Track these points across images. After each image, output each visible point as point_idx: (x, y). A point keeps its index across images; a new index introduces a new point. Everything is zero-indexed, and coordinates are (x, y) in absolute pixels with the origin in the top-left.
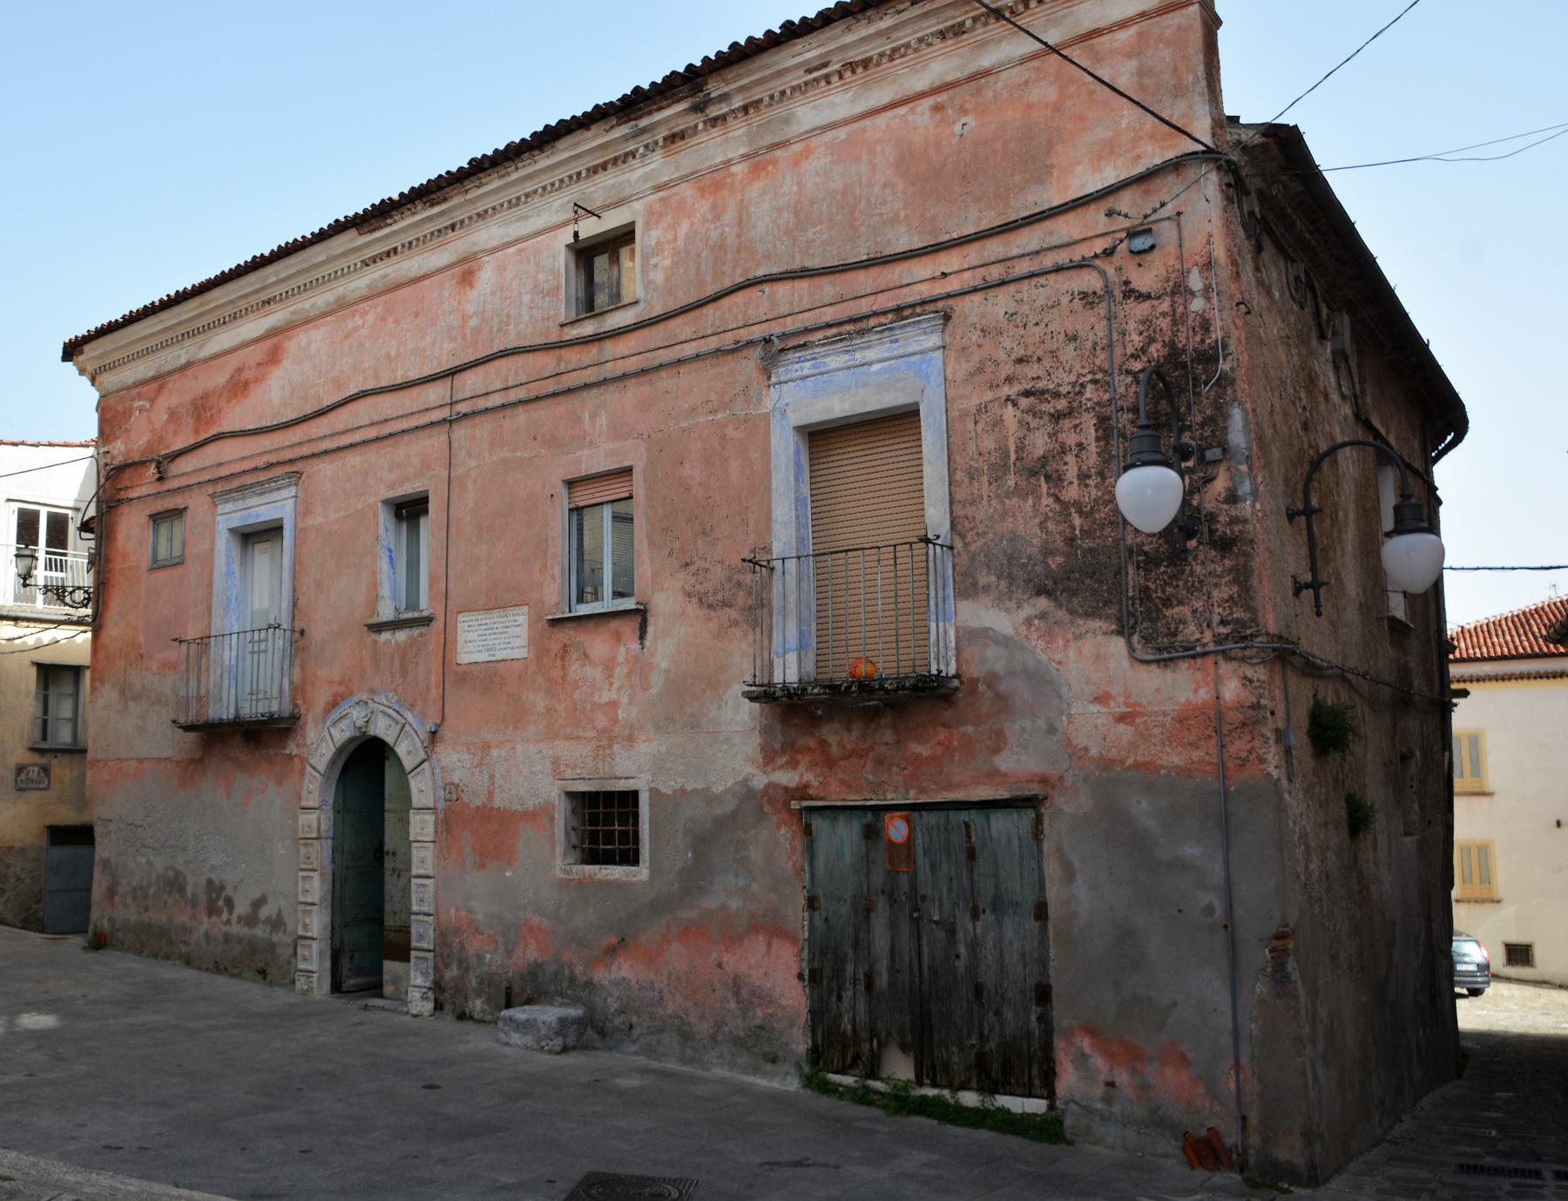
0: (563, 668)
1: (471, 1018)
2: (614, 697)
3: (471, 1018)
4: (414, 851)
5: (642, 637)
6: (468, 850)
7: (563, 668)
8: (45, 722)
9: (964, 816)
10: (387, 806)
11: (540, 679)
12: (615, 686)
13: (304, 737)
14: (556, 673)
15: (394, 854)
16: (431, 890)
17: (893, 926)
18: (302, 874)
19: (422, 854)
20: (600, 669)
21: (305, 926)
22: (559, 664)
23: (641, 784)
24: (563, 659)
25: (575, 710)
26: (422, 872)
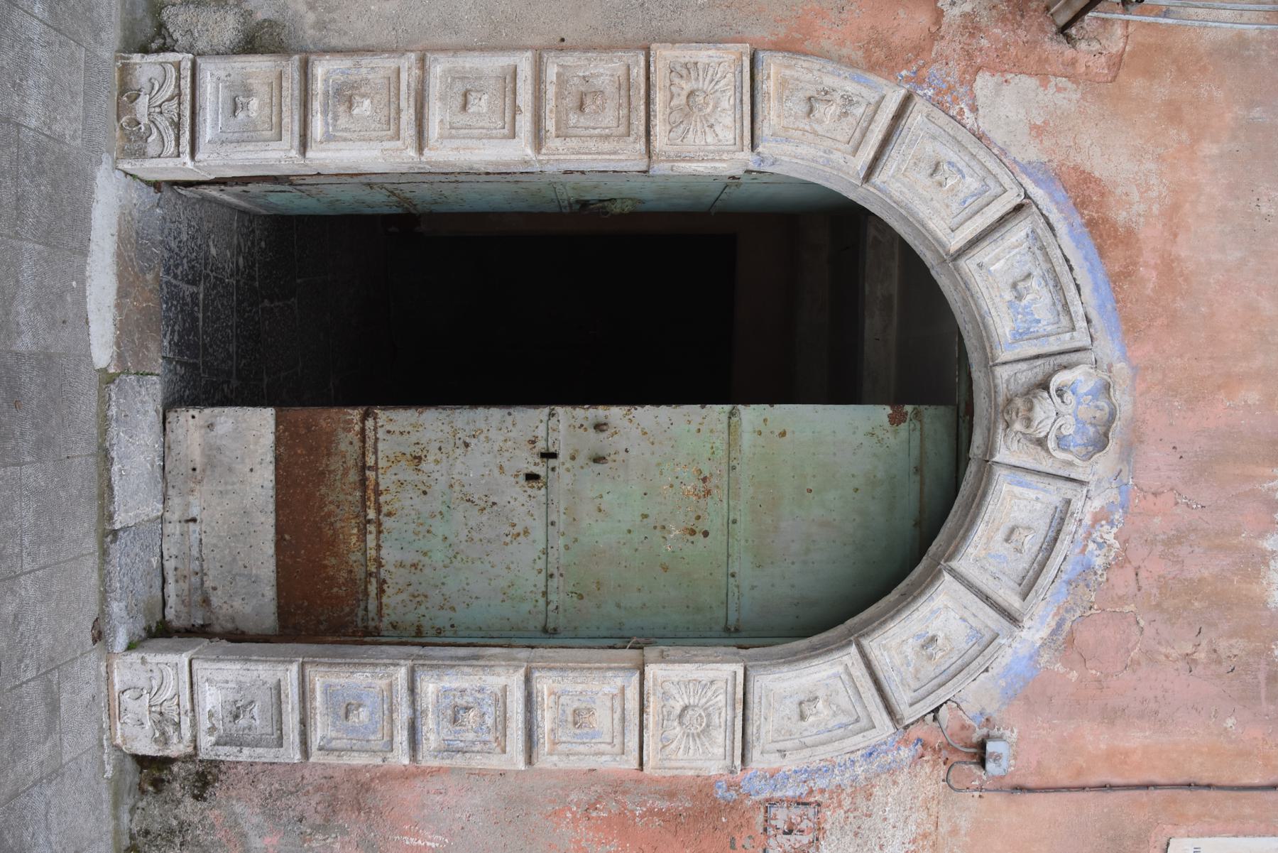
8: (1198, 786)
10: (751, 414)
13: (1003, 64)
16: (495, 762)
18: (524, 64)
19: (603, 719)
21: (345, 95)
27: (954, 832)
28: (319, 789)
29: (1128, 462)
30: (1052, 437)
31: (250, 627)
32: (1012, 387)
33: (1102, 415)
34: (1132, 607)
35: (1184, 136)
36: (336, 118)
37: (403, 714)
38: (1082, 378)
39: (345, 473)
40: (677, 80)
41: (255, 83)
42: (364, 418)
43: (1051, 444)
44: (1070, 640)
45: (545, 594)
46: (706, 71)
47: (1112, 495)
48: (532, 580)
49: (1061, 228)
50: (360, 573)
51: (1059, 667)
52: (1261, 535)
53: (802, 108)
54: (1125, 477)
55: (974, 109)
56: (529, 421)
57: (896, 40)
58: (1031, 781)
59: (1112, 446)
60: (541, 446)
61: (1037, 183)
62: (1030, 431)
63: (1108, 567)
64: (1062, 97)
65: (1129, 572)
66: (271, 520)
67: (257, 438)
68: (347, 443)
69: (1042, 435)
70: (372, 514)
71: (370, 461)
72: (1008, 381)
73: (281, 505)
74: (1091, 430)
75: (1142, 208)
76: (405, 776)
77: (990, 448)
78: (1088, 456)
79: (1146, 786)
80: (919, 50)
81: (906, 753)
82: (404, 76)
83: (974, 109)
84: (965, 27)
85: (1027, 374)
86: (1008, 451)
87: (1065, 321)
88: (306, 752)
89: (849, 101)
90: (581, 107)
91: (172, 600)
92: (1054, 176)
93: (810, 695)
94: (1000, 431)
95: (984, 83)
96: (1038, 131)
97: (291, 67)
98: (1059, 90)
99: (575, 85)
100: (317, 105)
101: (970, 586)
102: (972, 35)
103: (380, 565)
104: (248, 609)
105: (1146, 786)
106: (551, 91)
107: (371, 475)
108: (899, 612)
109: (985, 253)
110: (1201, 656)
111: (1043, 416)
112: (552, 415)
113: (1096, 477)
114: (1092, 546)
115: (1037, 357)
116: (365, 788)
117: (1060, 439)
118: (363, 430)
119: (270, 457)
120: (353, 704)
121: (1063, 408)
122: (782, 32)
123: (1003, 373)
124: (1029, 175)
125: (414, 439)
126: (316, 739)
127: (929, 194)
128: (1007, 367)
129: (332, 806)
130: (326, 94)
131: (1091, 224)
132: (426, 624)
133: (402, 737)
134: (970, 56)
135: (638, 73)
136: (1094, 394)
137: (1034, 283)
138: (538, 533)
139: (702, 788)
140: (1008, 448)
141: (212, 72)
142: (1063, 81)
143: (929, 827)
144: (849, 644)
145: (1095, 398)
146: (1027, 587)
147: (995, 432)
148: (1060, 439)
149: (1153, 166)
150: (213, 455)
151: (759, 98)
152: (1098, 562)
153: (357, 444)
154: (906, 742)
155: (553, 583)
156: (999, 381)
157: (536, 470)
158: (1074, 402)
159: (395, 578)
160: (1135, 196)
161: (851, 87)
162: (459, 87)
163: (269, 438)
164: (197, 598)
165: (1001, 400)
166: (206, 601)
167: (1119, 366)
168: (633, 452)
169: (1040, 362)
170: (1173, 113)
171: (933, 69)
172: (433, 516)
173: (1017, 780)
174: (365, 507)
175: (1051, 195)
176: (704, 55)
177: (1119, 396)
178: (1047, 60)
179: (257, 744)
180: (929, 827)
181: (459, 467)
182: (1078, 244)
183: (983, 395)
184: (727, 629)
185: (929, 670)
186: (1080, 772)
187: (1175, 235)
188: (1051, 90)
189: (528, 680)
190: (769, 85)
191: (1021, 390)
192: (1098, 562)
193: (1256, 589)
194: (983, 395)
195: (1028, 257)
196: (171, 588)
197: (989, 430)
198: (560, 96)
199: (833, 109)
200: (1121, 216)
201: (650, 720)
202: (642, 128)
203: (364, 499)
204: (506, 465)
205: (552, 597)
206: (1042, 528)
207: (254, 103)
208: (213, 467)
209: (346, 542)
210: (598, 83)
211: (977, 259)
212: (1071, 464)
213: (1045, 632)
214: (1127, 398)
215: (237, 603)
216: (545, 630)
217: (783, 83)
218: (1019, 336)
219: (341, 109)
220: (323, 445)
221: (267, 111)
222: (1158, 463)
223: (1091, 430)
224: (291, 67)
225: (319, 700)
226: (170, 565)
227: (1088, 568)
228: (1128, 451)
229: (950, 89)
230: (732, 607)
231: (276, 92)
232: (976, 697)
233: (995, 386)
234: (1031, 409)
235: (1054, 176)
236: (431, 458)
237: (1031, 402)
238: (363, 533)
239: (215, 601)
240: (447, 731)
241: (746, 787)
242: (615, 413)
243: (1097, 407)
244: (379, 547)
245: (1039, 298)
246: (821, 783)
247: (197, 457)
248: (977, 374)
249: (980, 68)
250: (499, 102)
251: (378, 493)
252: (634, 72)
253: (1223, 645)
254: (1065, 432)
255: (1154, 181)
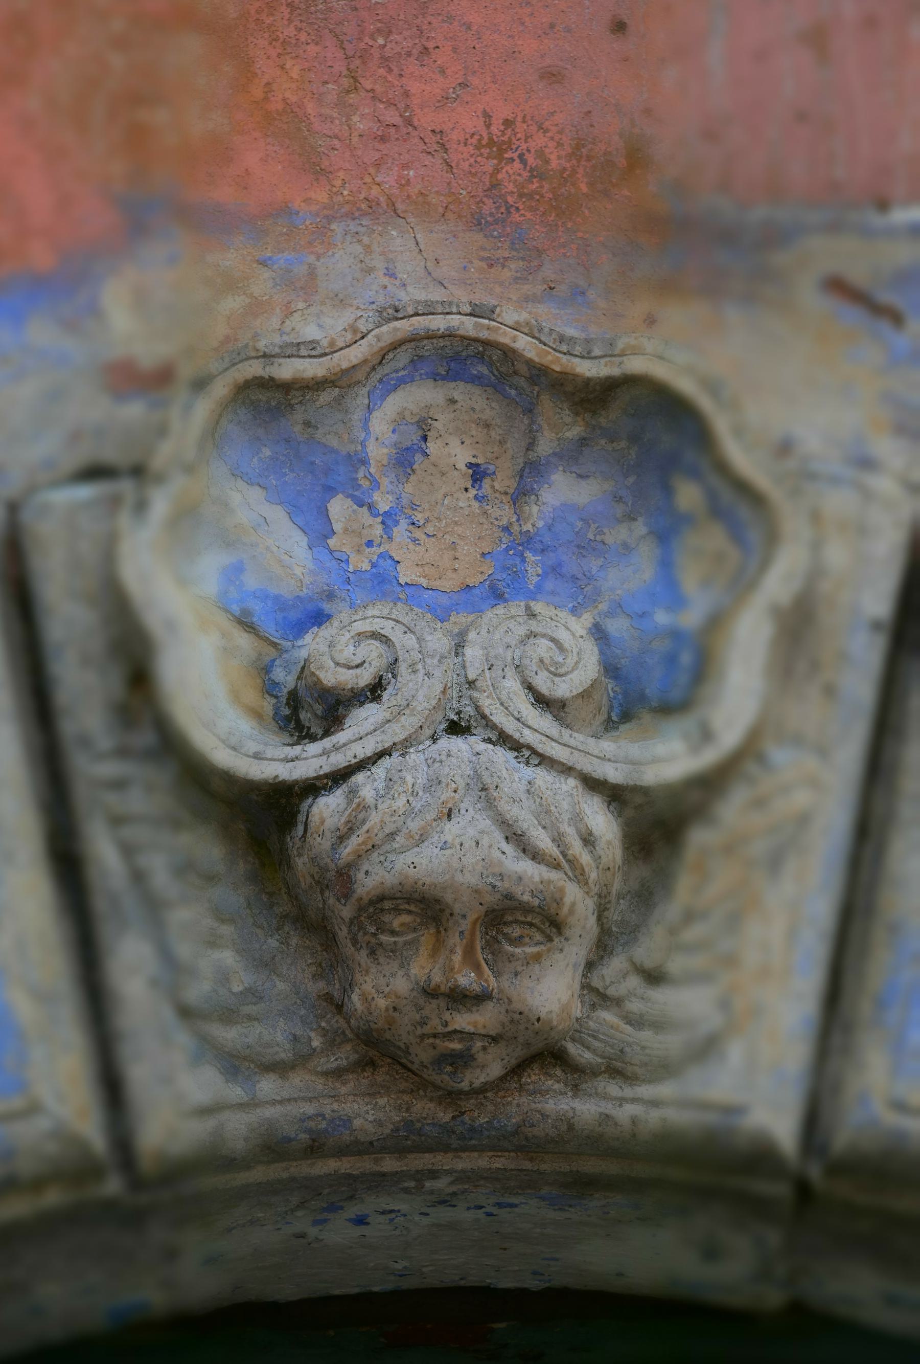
29: (775, 237)
30: (621, 757)
32: (274, 1035)
34: (497, 636)
38: (210, 567)
43: (664, 758)
59: (668, 349)
62: (578, 903)
69: (602, 821)
72: (235, 1064)
74: (562, 492)
77: (710, 1172)
78: (743, 510)
85: (187, 939)
94: (585, 1109)
111: (471, 828)
113: (889, 450)
115: (67, 862)
117: (631, 698)
121: (421, 690)
123: (183, 1100)
128: (140, 1074)
136: (316, 482)
140: (707, 1049)
145: (341, 473)
147: (597, 1142)
148: (631, 698)
156: (238, 1128)
158: (375, 617)
165: (366, 1112)
167: (126, 316)
169: (103, 851)
177: (327, 328)
183: (338, 1232)
191: (296, 977)
194: (338, 1232)
197: (583, 1185)
212: (798, 626)
214: (339, 262)
223: (562, 492)
228: (701, 243)
233: (273, 1148)
234: (426, 907)
237: (382, 903)
243: (404, 460)
248: (194, 1270)
254: (581, 671)
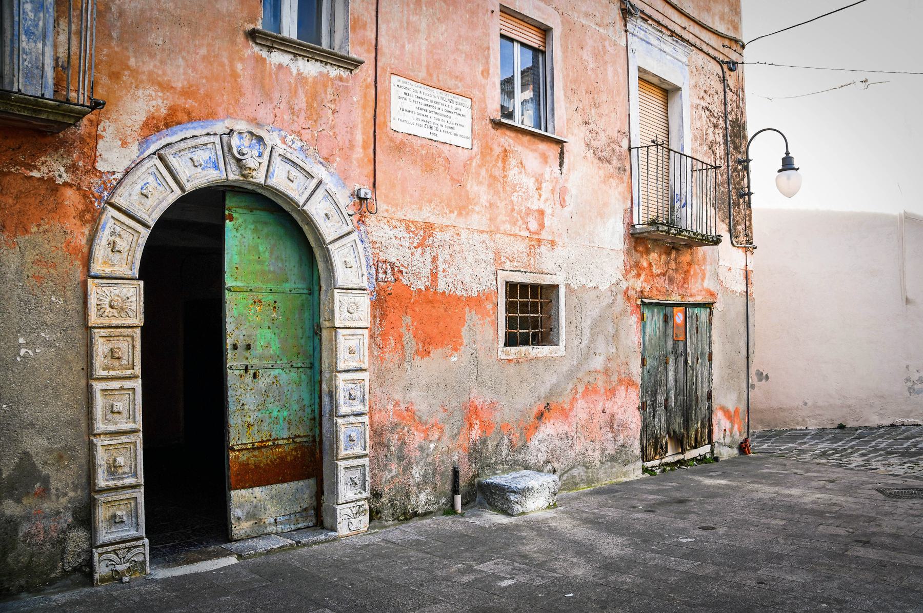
0: (504, 169)
1: (415, 514)
2: (542, 207)
3: (415, 514)
4: (341, 339)
5: (561, 165)
6: (407, 337)
7: (504, 169)
9: (696, 310)
10: (229, 282)
11: (483, 172)
12: (543, 198)
14: (497, 172)
15: (553, 243)
17: (676, 370)
19: (353, 343)
20: (533, 179)
22: (500, 164)
23: (558, 279)
24: (504, 161)
25: (513, 210)
26: (353, 365)
27: (387, 211)
28: (376, 450)
31: (314, 489)
33: (249, 136)
35: (126, 73)
36: (124, 473)
37: (352, 419)
39: (255, 456)
40: (106, 314)
41: (109, 514)
42: (234, 451)
44: (326, 159)
45: (298, 368)
46: (101, 300)
47: (276, 134)
48: (293, 375)
49: (168, 140)
50: (292, 446)
51: (335, 165)
52: (291, 73)
53: (117, 255)
54: (269, 128)
55: (114, 173)
56: (232, 377)
57: (81, 207)
58: (372, 180)
60: (242, 372)
61: (148, 148)
63: (301, 140)
64: (108, 129)
65: (303, 132)
66: (274, 486)
67: (243, 497)
68: (243, 457)
70: (271, 443)
71: (250, 446)
73: (268, 483)
75: (160, 102)
76: (371, 418)
79: (375, 136)
80: (85, 196)
81: (362, 228)
82: (106, 443)
83: (114, 173)
84: (73, 172)
85: (232, 166)
86: (259, 177)
87: (210, 146)
88: (366, 456)
89: (113, 233)
90: (119, 358)
91: (306, 524)
92: (144, 141)
93: (348, 266)
95: (101, 166)
96: (124, 144)
97: (101, 498)
98: (104, 130)
99: (109, 361)
100: (120, 483)
101: (308, 199)
102: (78, 169)
103: (290, 438)
104: (308, 491)
105: (375, 136)
106: (112, 373)
107: (256, 445)
108: (317, 228)
109: (183, 178)
110: (333, 107)
112: (231, 368)
114: (293, 146)
116: (375, 432)
118: (238, 450)
119: (250, 490)
120: (350, 437)
121: (250, 154)
122: (78, 263)
123: (232, 177)
124: (144, 151)
125: (241, 428)
126: (363, 452)
127: (150, 196)
129: (381, 444)
130: (113, 479)
131: (167, 126)
132: (310, 417)
133: (360, 419)
134: (87, 172)
135: (103, 332)
137: (195, 158)
138: (277, 371)
139: (374, 304)
141: (104, 536)
142: (100, 128)
143: (385, 221)
144: (327, 248)
146: (310, 176)
149: (141, 92)
150: (251, 516)
151: (114, 275)
152: (299, 144)
153: (244, 452)
154: (359, 227)
155: (294, 365)
157: (252, 376)
159: (295, 431)
160: (154, 103)
161: (107, 231)
162: (110, 416)
163: (243, 492)
164: (304, 514)
166: (305, 509)
168: (245, 333)
170: (115, 76)
171: (94, 190)
172: (271, 417)
173: (371, 185)
174: (268, 447)
175: (153, 142)
176: (93, 301)
178: (89, 134)
179: (364, 475)
180: (385, 221)
181: (252, 407)
182: (174, 133)
184: (310, 294)
185: (336, 217)
186: (369, 161)
187: (172, 87)
188: (103, 134)
189: (340, 372)
190: (108, 271)
192: (299, 144)
193: (310, 80)
195: (183, 158)
196: (301, 525)
198: (114, 369)
199: (118, 240)
200: (164, 111)
201: (353, 325)
202: (129, 330)
203: (266, 447)
204: (250, 387)
205: (299, 365)
206: (289, 167)
207: (119, 513)
208: (255, 515)
209: (281, 453)
210: (107, 351)
211: (185, 182)
213: (323, 169)
215: (306, 496)
216: (311, 368)
217: (105, 264)
218: (216, 167)
219: (120, 471)
220: (244, 466)
221: (122, 507)
222: (264, 113)
224: (101, 498)
225: (349, 452)
226: (293, 527)
227: (301, 148)
229: (104, 183)
230: (302, 291)
231: (113, 504)
232: (344, 199)
235: (144, 141)
236: (248, 419)
238: (279, 446)
239: (305, 506)
240: (357, 402)
241: (372, 289)
242: (229, 341)
244: (283, 439)
245: (202, 156)
246: (371, 261)
247: (250, 523)
249: (94, 168)
250: (117, 397)
251: (263, 441)
252: (104, 334)
253: (330, 97)
255: (147, 92)
